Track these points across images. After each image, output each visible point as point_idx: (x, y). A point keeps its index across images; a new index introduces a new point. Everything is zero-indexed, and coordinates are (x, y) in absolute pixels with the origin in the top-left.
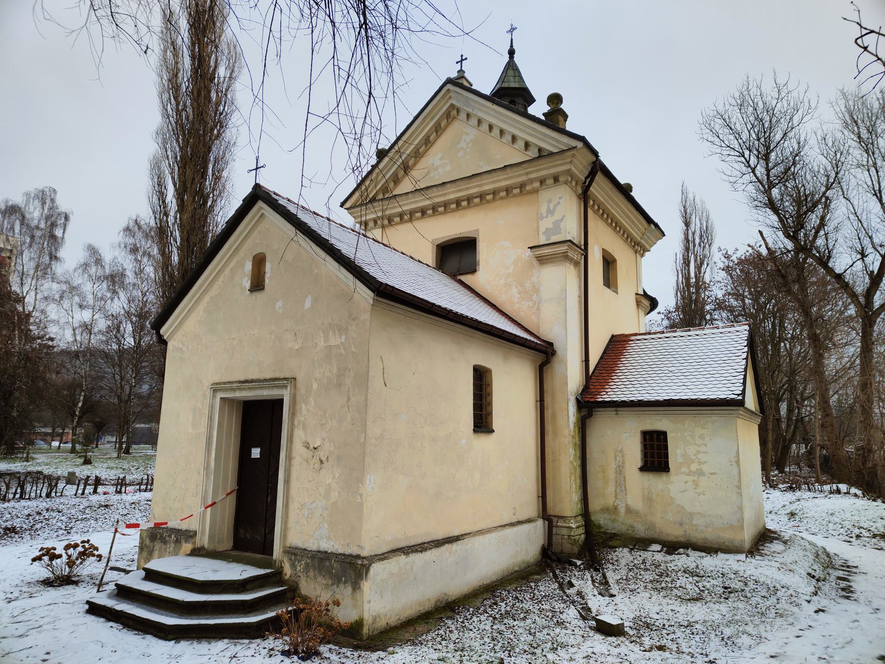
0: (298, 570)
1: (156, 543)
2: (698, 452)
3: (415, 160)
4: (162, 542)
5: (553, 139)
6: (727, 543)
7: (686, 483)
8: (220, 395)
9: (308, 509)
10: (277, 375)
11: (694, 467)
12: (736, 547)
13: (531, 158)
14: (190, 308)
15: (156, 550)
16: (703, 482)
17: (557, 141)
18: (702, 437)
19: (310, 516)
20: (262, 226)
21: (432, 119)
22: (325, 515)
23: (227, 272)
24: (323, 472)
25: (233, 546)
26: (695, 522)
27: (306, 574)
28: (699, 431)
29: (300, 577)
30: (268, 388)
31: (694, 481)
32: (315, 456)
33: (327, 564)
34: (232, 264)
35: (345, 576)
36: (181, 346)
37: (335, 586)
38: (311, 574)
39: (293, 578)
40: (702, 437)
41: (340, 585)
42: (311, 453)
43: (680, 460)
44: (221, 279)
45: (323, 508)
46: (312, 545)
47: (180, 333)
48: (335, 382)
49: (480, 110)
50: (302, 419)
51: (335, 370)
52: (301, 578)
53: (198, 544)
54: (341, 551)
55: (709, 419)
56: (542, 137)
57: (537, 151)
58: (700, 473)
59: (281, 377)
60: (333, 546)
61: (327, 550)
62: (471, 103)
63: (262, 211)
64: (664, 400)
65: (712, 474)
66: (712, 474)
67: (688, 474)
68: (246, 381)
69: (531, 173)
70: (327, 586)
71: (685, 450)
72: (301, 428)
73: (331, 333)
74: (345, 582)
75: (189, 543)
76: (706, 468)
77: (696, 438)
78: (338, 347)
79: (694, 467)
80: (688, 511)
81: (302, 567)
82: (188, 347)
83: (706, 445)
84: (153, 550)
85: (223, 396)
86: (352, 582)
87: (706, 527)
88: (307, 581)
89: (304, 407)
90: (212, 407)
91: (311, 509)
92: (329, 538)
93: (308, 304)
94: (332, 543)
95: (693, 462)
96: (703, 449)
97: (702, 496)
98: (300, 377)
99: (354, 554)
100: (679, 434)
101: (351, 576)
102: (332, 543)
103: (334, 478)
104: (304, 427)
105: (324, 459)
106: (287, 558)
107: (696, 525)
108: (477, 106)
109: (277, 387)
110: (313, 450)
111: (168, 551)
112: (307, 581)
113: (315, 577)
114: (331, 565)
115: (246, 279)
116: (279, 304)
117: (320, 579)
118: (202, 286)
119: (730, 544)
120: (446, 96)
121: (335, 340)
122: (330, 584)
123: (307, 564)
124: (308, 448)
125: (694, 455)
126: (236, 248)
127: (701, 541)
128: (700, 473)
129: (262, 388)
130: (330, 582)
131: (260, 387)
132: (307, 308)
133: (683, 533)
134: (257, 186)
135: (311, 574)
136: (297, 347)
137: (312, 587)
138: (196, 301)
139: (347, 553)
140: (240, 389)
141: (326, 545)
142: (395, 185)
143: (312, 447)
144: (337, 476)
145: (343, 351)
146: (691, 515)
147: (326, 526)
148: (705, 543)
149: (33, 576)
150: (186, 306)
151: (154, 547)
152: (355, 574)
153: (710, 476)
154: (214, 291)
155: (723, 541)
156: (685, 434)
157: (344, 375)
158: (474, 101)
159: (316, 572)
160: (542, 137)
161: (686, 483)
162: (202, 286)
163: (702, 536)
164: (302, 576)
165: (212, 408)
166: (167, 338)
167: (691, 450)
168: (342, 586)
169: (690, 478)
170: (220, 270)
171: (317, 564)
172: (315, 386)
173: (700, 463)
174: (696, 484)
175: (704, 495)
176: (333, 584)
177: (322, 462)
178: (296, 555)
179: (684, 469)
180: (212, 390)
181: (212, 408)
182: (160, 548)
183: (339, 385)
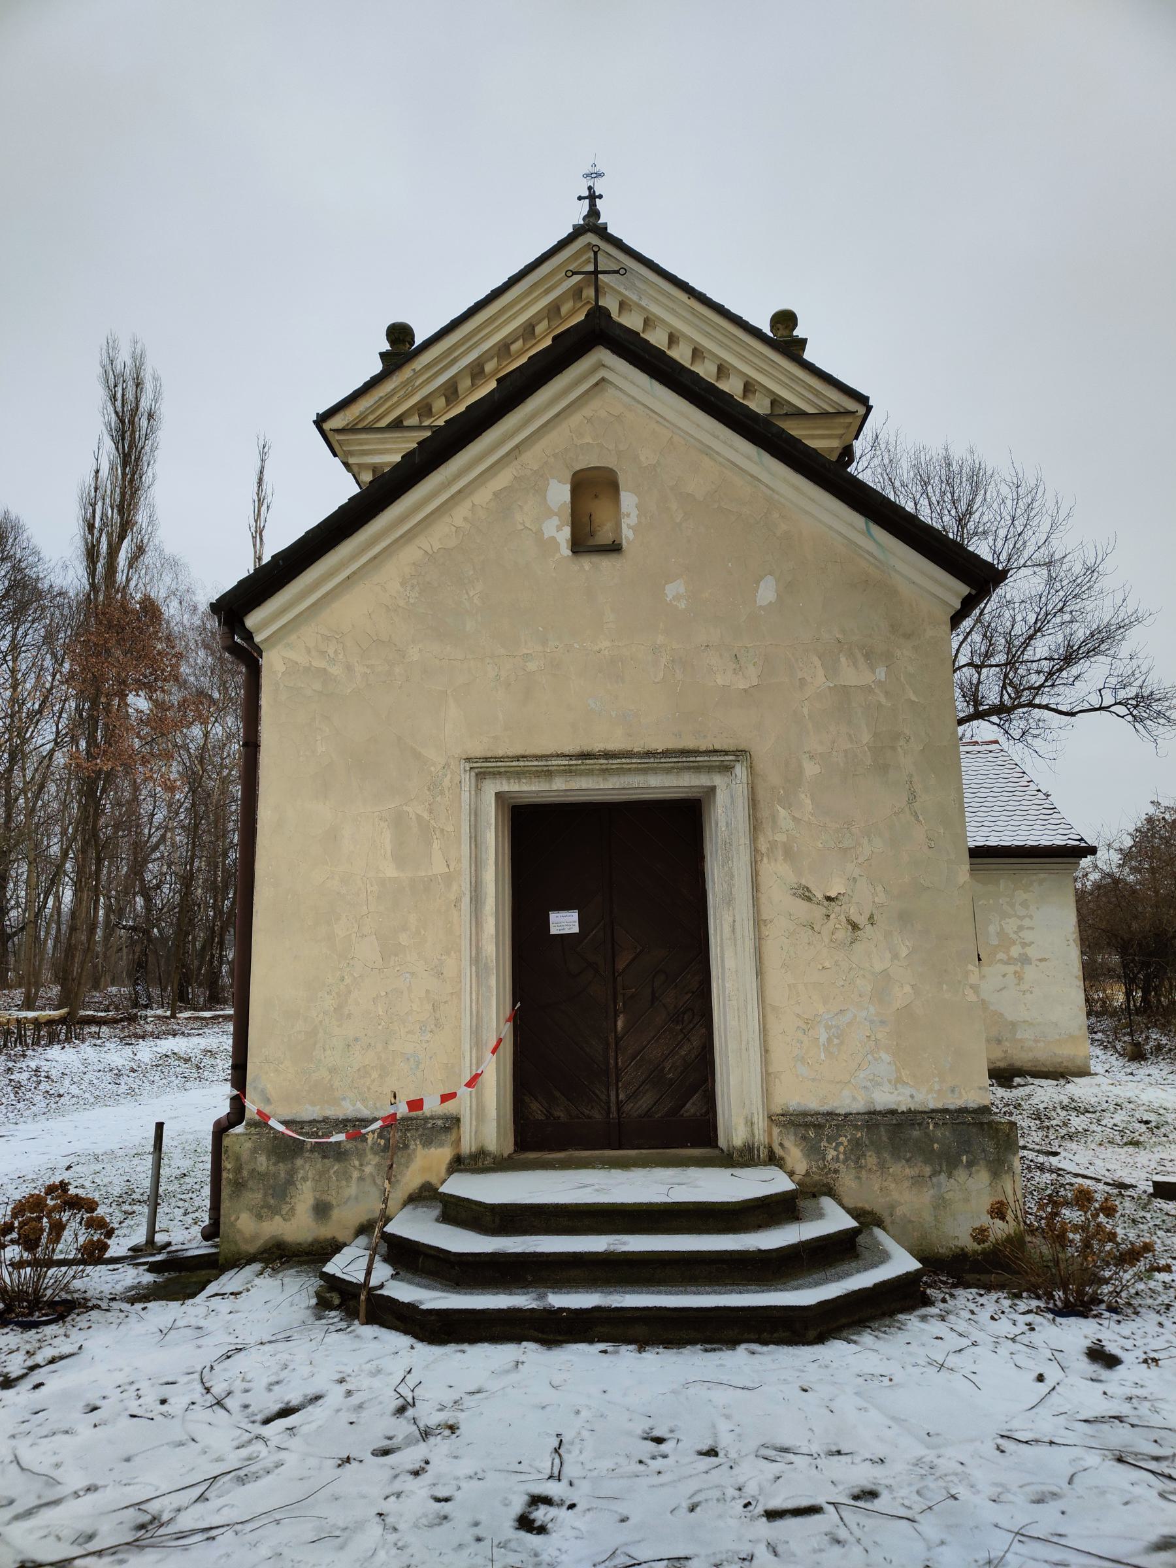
0: (829, 1157)
1: (299, 1162)
2: (1021, 928)
3: (499, 365)
4: (324, 1157)
5: (810, 388)
6: (1065, 1064)
7: (1004, 976)
8: (491, 788)
9: (828, 1028)
10: (689, 743)
11: (1015, 951)
12: (1079, 1067)
13: (816, 411)
14: (354, 573)
15: (305, 1179)
16: (1030, 972)
17: (817, 393)
18: (1024, 904)
19: (836, 1041)
20: (596, 407)
21: (547, 292)
22: (879, 1036)
23: (483, 496)
24: (859, 947)
25: (516, 1144)
26: (1019, 1036)
27: (857, 1162)
28: (1021, 895)
29: (836, 1171)
30: (668, 771)
31: (1015, 973)
32: (832, 916)
33: (916, 1133)
34: (503, 479)
35: (967, 1152)
36: (321, 664)
37: (943, 1177)
38: (871, 1160)
39: (816, 1178)
40: (1024, 904)
41: (955, 1173)
42: (818, 912)
43: (994, 941)
44: (461, 513)
45: (871, 1022)
46: (850, 1100)
47: (309, 634)
48: (869, 762)
49: (656, 301)
50: (781, 838)
51: (866, 737)
52: (842, 1175)
53: (468, 1145)
54: (932, 1105)
55: (1034, 877)
56: (787, 381)
57: (767, 402)
58: (1025, 960)
59: (703, 748)
60: (912, 1096)
61: (894, 1107)
62: (639, 284)
63: (602, 373)
64: (976, 847)
65: (1041, 960)
66: (1041, 960)
67: (1007, 963)
68: (585, 756)
69: (371, 454)
70: (918, 1181)
71: (1001, 925)
72: (781, 858)
73: (843, 659)
74: (970, 1164)
75: (441, 1145)
76: (1031, 952)
77: (1017, 905)
78: (868, 689)
79: (1015, 951)
80: (1010, 1019)
81: (841, 1149)
82: (349, 668)
83: (1031, 917)
84: (290, 1182)
85: (500, 789)
86: (989, 1162)
87: (1036, 1041)
88: (859, 1178)
89: (782, 812)
90: (475, 813)
91: (838, 1027)
92: (898, 1081)
93: (767, 593)
94: (908, 1091)
95: (1014, 943)
96: (1027, 922)
97: (1028, 995)
98: (763, 749)
99: (973, 1105)
100: (991, 902)
101: (984, 1151)
102: (908, 1091)
103: (895, 956)
104: (789, 854)
105: (861, 920)
106: (793, 1138)
107: (1021, 1040)
108: (652, 292)
109: (698, 769)
110: (826, 903)
111: (356, 1174)
112: (859, 1178)
113: (882, 1166)
114: (927, 1135)
115: (555, 521)
116: (674, 589)
117: (896, 1168)
118: (402, 519)
119: (1069, 1065)
120: (581, 256)
121: (853, 675)
122: (928, 1174)
123: (856, 1144)
124: (809, 899)
125: (1015, 933)
126: (517, 447)
127: (1030, 1064)
128: (1025, 960)
129: (645, 771)
130: (928, 1170)
131: (641, 769)
132: (765, 603)
133: (1003, 1055)
134: (598, 314)
135: (871, 1160)
136: (742, 685)
137: (876, 1187)
138: (375, 558)
139: (952, 1107)
140: (569, 772)
141: (887, 1098)
142: (447, 405)
143: (820, 896)
144: (904, 952)
145: (883, 700)
146: (1014, 1025)
147: (886, 1057)
148: (1036, 1066)
149: (1107, 1174)
150: (343, 565)
151: (292, 1173)
152: (997, 1144)
153: (1038, 963)
154: (438, 537)
155: (1060, 1060)
156: (1001, 901)
157: (894, 749)
158: (646, 281)
159: (886, 1155)
160: (787, 381)
161: (1004, 976)
162: (402, 519)
163: (1031, 1055)
164: (842, 1168)
165: (476, 815)
166: (266, 640)
167: (1010, 925)
168: (961, 1174)
169: (1011, 969)
170: (460, 491)
171: (885, 1139)
172: (811, 769)
173: (1024, 945)
174: (1019, 977)
175: (1031, 993)
176: (935, 1173)
177: (855, 927)
178: (818, 1127)
179: (1001, 956)
180: (473, 774)
181: (476, 815)
182: (321, 1174)
183: (882, 768)
